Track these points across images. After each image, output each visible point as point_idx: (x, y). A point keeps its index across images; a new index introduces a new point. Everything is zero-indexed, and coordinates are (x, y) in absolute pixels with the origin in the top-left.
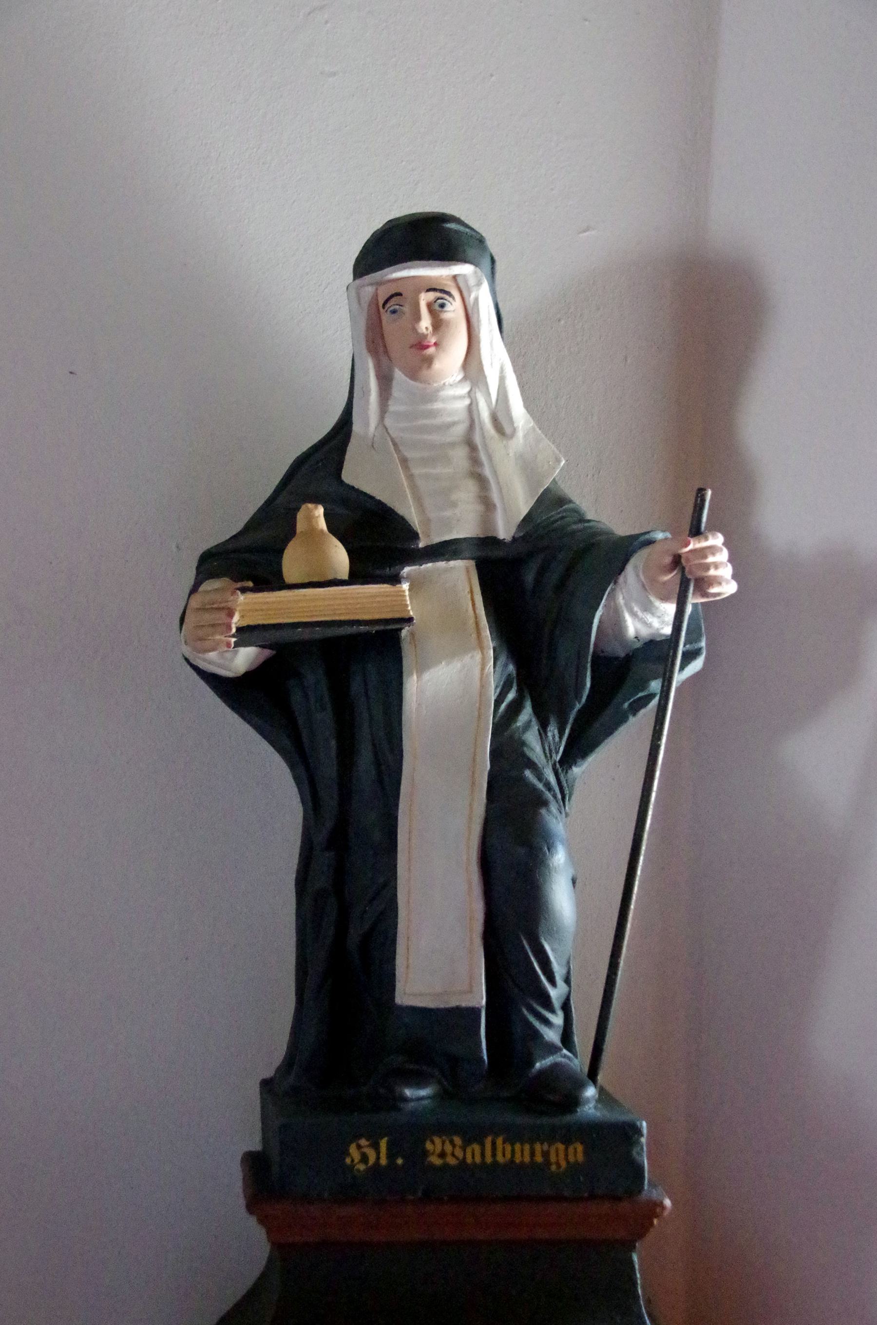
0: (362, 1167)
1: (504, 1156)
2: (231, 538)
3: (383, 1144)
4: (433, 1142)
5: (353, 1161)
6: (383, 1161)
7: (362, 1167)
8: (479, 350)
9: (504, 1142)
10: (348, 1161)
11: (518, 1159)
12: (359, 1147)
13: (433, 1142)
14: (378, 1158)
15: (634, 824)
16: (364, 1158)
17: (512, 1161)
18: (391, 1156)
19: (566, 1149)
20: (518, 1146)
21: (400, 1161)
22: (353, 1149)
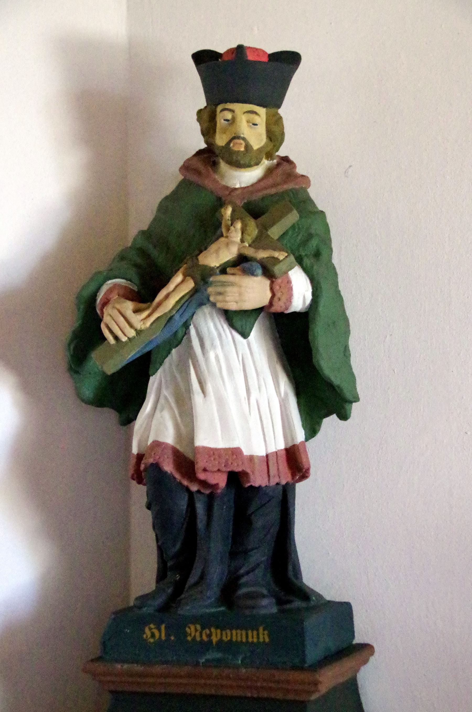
0: (152, 640)
1: (226, 637)
2: (192, 407)
3: (163, 627)
4: (189, 628)
5: (147, 637)
6: (163, 637)
7: (152, 640)
8: (308, 588)
9: (264, 630)
10: (145, 636)
11: (234, 639)
12: (150, 629)
13: (189, 628)
14: (160, 635)
15: (244, 382)
16: (153, 635)
17: (231, 640)
18: (168, 635)
19: (222, 637)
20: (224, 633)
21: (172, 638)
22: (147, 630)
